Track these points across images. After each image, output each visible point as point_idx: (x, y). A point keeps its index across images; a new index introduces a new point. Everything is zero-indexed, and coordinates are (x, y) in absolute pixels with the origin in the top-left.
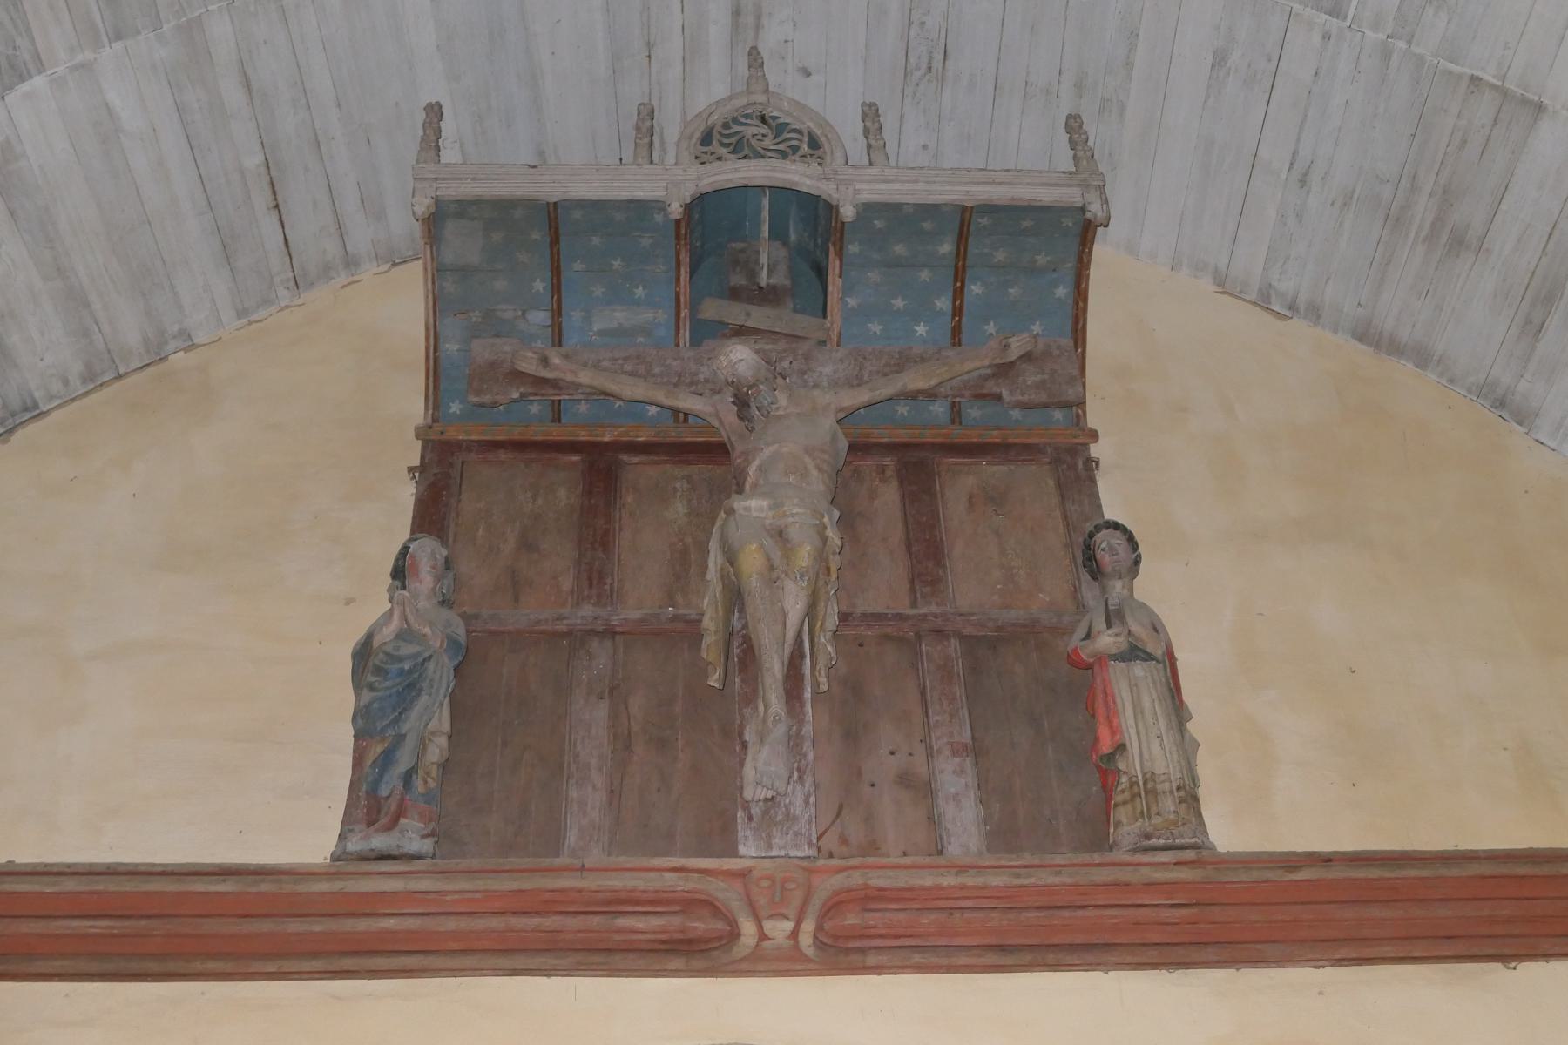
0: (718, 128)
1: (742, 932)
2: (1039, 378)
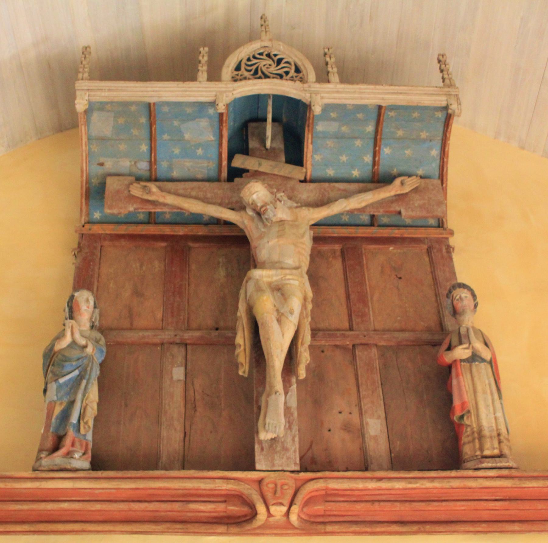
1: (258, 512)
2: (421, 202)
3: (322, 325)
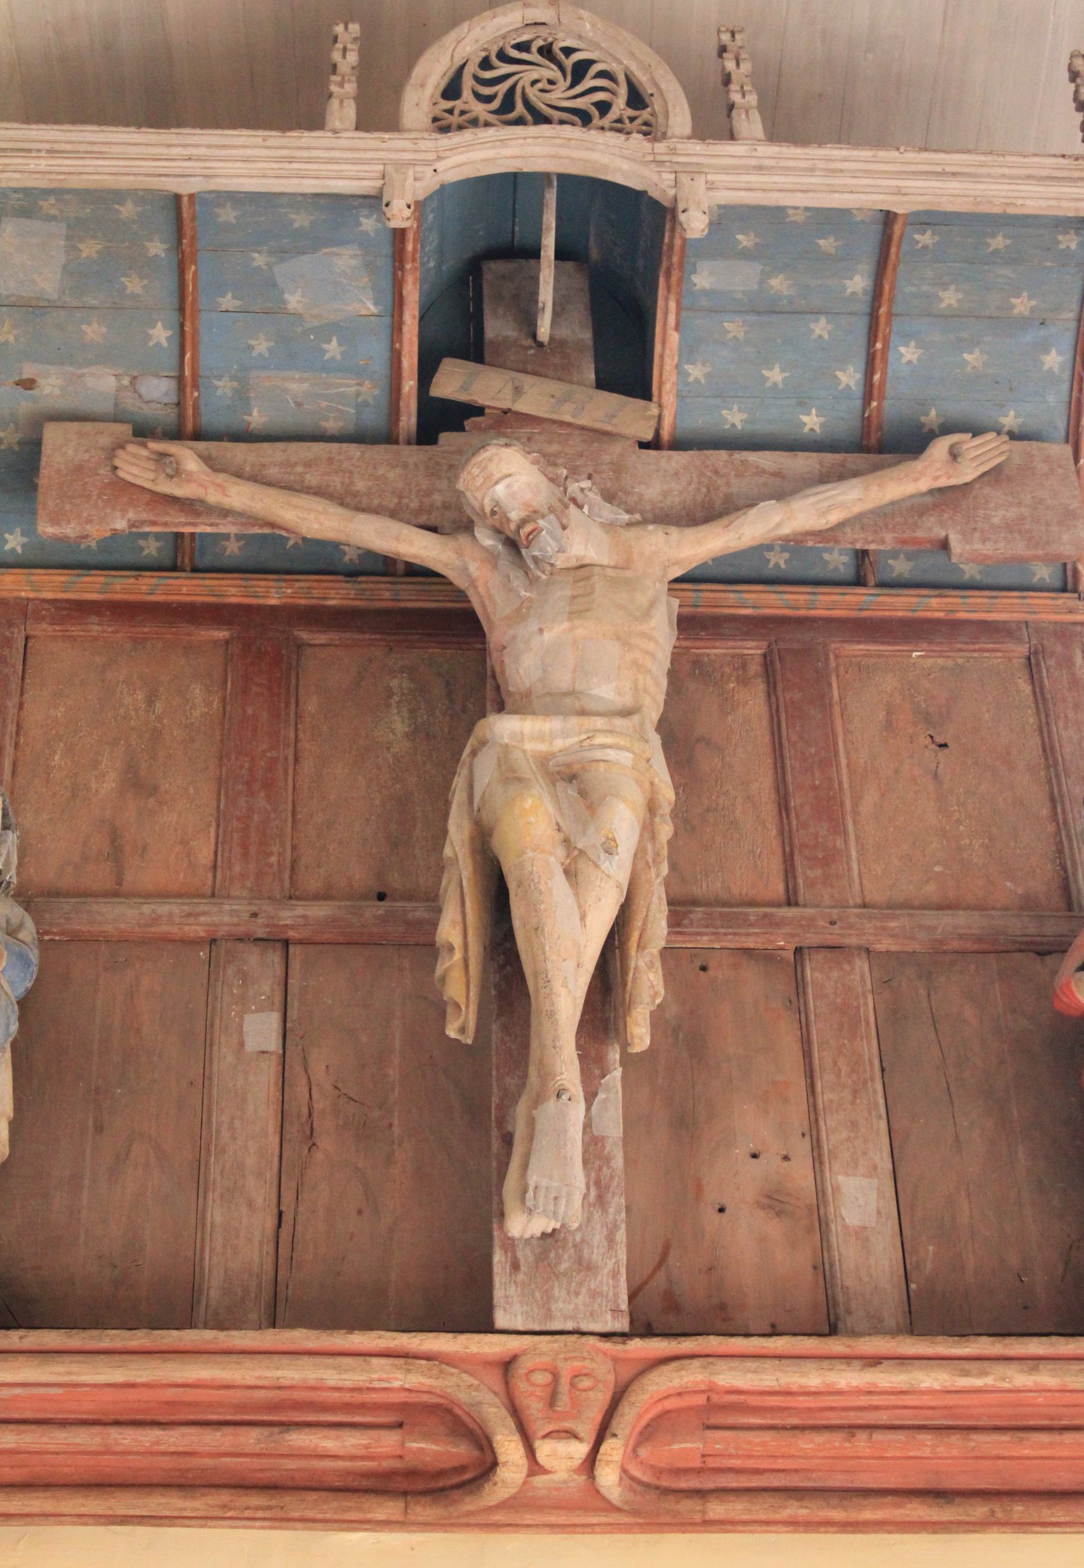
0: (471, 69)
3: (699, 890)
